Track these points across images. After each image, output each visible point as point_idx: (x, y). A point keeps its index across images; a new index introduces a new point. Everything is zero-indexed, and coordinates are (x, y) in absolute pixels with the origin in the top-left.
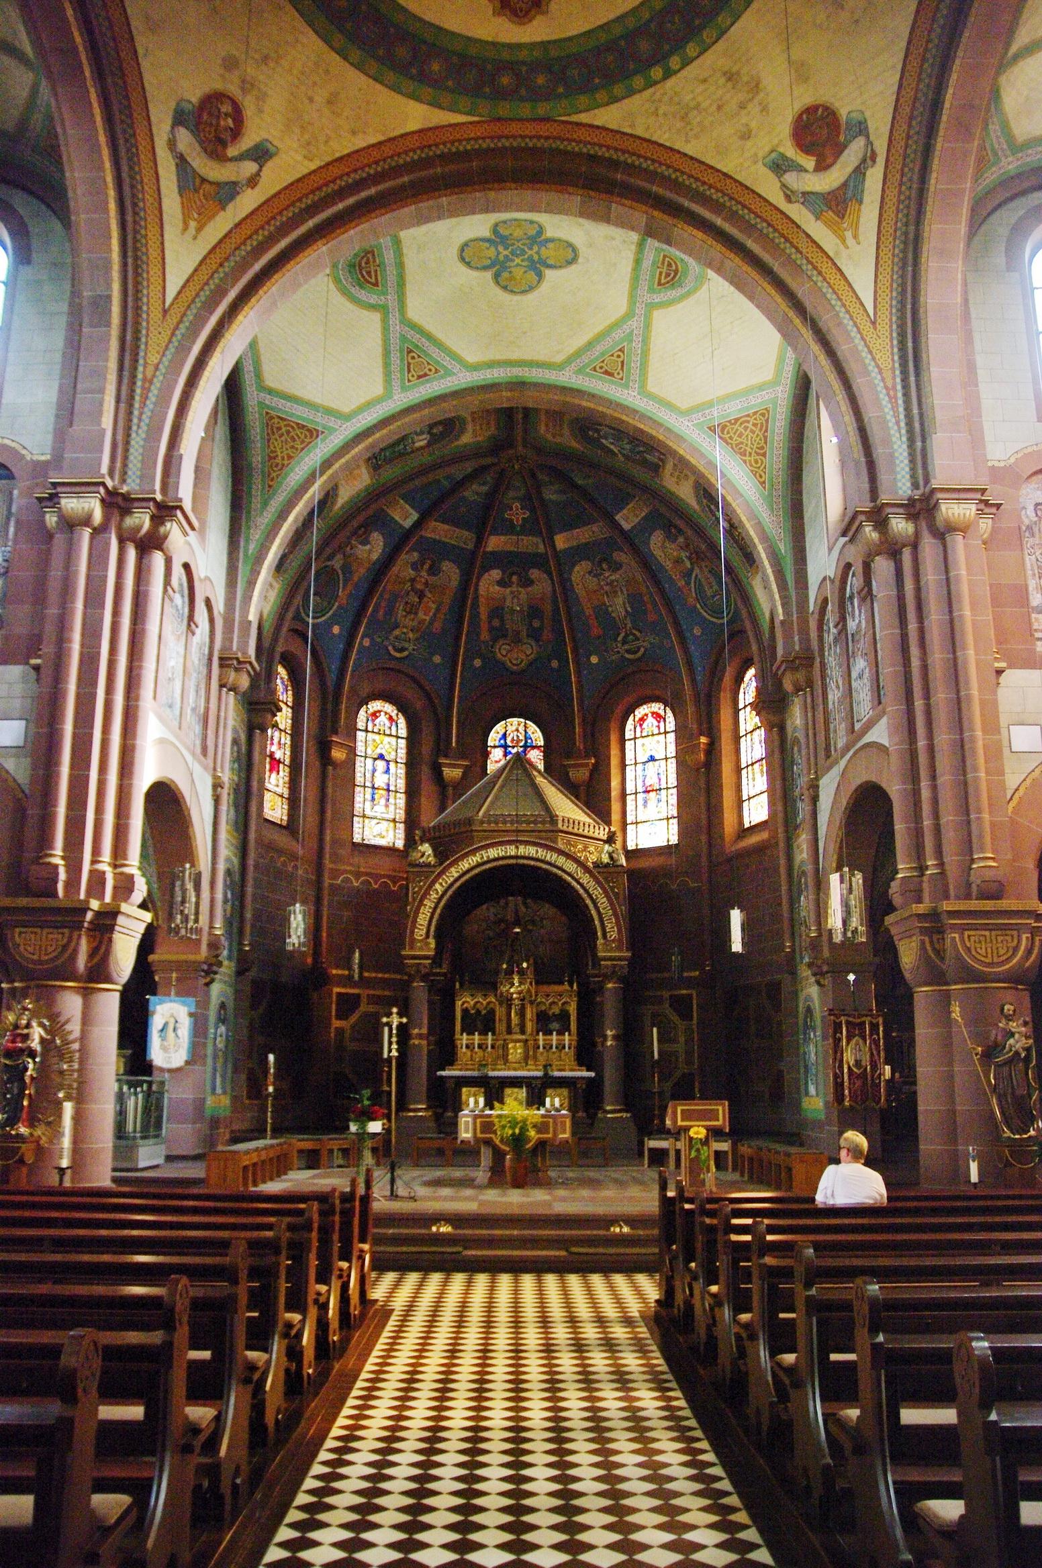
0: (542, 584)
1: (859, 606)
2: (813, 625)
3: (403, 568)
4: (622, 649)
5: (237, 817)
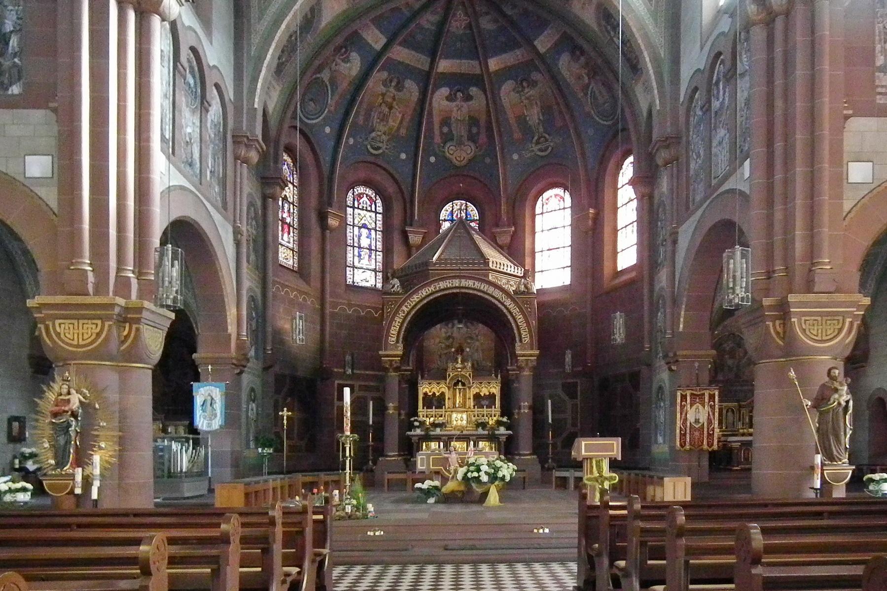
0: (479, 100)
1: (724, 88)
2: (682, 112)
3: (376, 82)
4: (535, 148)
5: (257, 260)
